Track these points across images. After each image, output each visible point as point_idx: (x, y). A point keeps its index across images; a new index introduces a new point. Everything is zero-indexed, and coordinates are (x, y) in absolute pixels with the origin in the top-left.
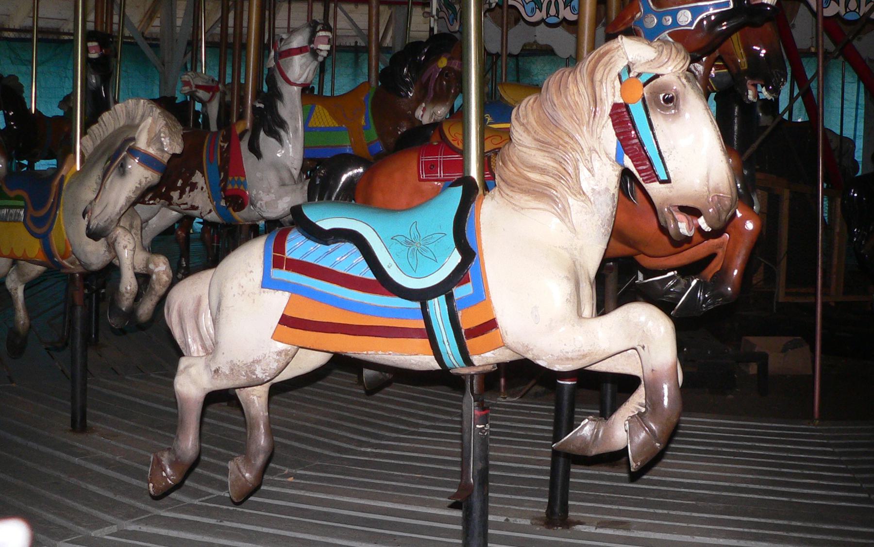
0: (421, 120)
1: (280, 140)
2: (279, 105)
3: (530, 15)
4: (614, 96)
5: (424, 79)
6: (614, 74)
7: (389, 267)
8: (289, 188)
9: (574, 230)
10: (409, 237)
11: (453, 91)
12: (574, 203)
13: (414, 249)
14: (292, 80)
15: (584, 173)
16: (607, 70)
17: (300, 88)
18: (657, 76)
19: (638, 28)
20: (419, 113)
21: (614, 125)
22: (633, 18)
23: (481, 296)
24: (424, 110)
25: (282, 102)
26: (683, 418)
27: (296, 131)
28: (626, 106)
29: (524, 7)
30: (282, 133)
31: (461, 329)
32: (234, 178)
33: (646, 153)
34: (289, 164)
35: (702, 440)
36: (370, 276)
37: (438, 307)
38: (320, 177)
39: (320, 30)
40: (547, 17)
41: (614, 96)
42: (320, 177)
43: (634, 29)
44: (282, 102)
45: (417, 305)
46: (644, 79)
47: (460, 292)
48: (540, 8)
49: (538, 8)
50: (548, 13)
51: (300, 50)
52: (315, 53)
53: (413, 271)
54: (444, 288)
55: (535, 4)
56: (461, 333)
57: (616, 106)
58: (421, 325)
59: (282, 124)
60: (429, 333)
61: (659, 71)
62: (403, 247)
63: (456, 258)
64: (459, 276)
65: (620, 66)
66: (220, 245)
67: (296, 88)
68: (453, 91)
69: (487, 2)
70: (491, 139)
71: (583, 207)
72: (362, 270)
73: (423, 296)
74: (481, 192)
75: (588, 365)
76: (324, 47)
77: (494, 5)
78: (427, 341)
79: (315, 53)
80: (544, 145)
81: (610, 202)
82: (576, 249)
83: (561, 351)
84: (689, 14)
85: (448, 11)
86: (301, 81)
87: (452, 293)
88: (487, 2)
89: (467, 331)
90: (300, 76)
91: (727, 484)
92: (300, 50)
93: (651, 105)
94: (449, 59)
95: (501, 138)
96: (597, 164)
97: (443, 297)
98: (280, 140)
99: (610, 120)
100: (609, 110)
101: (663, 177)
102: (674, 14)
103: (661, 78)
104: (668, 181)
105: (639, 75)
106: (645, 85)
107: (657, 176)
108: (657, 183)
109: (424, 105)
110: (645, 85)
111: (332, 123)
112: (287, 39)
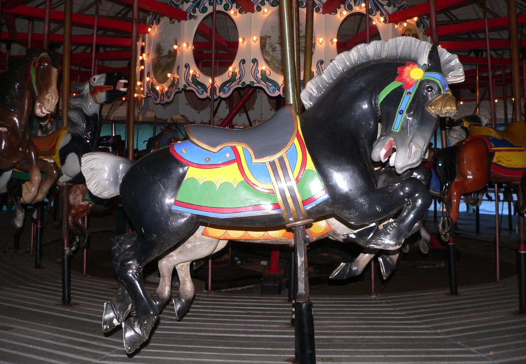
0: (46, 115)
3: (201, 94)
11: (468, 140)
20: (38, 112)
26: (310, 298)
29: (268, 88)
32: (238, 260)
48: (279, 89)
49: (278, 90)
55: (275, 87)
66: (129, 334)
68: (468, 140)
69: (177, 88)
75: (216, 246)
77: (181, 90)
85: (265, 83)
88: (177, 88)
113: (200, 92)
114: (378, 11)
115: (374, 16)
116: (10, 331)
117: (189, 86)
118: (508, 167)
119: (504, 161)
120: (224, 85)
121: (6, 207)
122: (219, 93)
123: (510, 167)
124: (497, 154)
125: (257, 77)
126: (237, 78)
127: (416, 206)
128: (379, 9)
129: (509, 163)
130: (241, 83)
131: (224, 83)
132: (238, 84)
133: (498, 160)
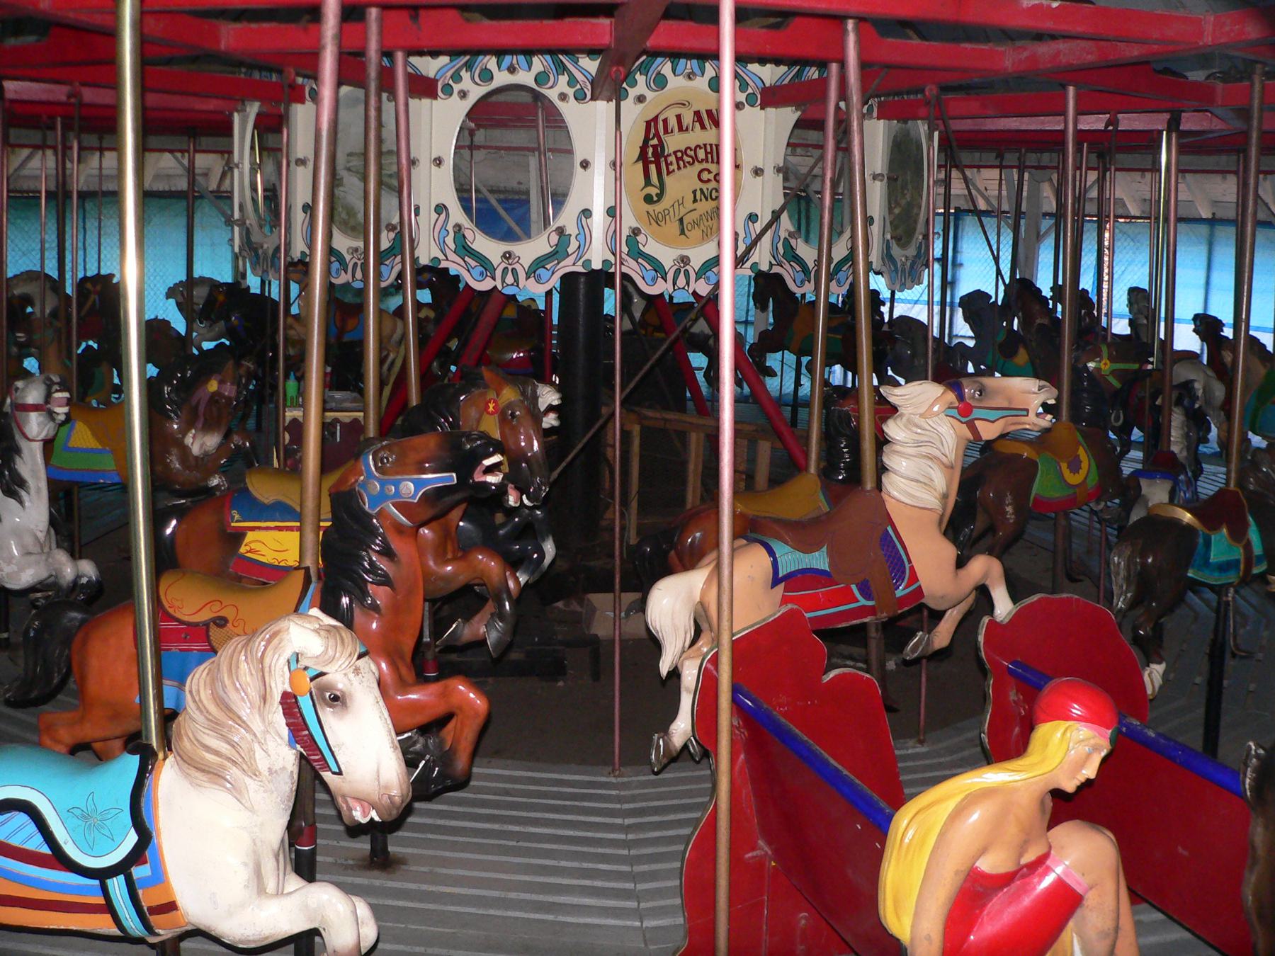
1: (21, 502)
2: (18, 460)
4: (284, 683)
5: (194, 401)
6: (283, 661)
7: (65, 843)
8: (33, 558)
9: (252, 810)
10: (85, 810)
12: (251, 784)
13: (90, 824)
14: (30, 437)
15: (259, 754)
16: (276, 656)
17: (42, 443)
18: (322, 674)
19: (362, 491)
21: (284, 714)
22: (356, 481)
23: (159, 876)
24: (194, 438)
25: (20, 456)
27: (39, 490)
28: (295, 697)
30: (23, 493)
31: (142, 907)
33: (216, 940)
34: (32, 526)
35: (484, 874)
36: (46, 850)
37: (117, 885)
38: (34, 629)
39: (57, 391)
40: (353, 281)
41: (284, 683)
42: (34, 629)
43: (359, 491)
44: (20, 456)
45: (97, 882)
46: (312, 673)
47: (139, 872)
49: (662, 278)
50: (353, 276)
51: (35, 408)
52: (51, 415)
53: (90, 850)
54: (122, 868)
56: (143, 910)
57: (285, 695)
58: (101, 901)
59: (22, 483)
60: (109, 908)
61: (324, 670)
62: (80, 822)
63: (132, 838)
64: (137, 856)
65: (288, 653)
67: (38, 443)
70: (209, 605)
71: (260, 786)
72: (36, 844)
73: (102, 875)
74: (161, 756)
76: (62, 411)
78: (109, 916)
79: (51, 415)
80: (216, 726)
81: (289, 781)
82: (256, 826)
83: (242, 935)
84: (411, 485)
86: (42, 436)
87: (131, 873)
89: (150, 909)
90: (39, 434)
91: (586, 804)
92: (35, 408)
93: (319, 703)
94: (221, 382)
95: (221, 603)
96: (271, 745)
97: (121, 877)
98: (21, 502)
99: (280, 707)
100: (279, 698)
101: (335, 769)
102: (397, 485)
103: (324, 678)
104: (340, 773)
105: (306, 668)
106: (312, 679)
107: (329, 766)
108: (329, 773)
109: (193, 431)
110: (312, 679)
111: (92, 443)
112: (23, 389)
113: (649, 280)
114: (564, 74)
115: (551, 87)
116: (189, 942)
117: (447, 259)
118: (276, 563)
119: (263, 550)
120: (540, 263)
121: (1044, 294)
122: (696, 281)
123: (282, 564)
124: (250, 536)
125: (444, 242)
126: (570, 250)
127: (1046, 297)
128: (565, 68)
129: (280, 556)
130: (580, 263)
131: (538, 261)
132: (574, 264)
133: (248, 549)
